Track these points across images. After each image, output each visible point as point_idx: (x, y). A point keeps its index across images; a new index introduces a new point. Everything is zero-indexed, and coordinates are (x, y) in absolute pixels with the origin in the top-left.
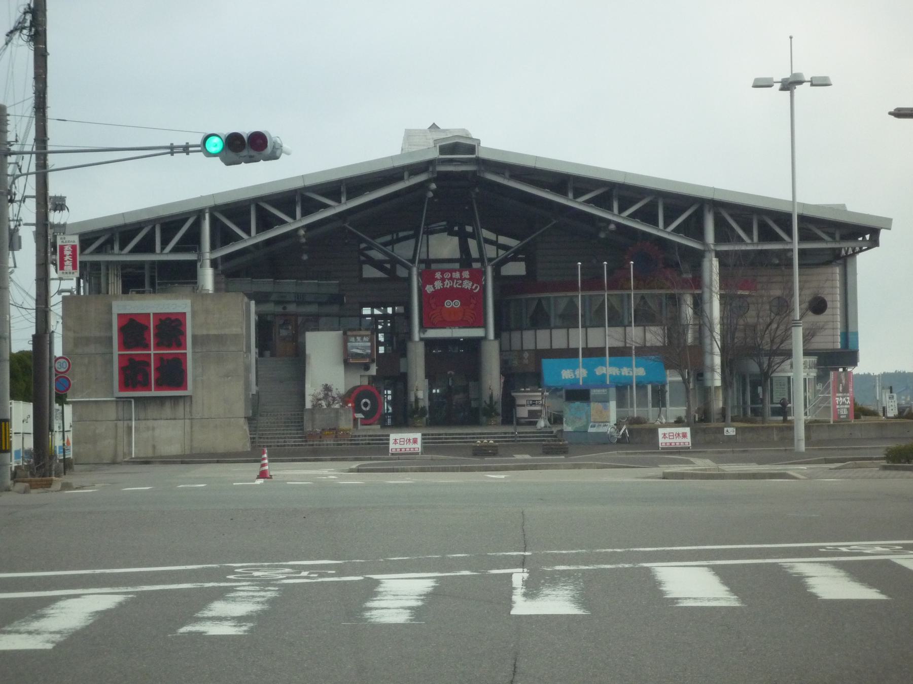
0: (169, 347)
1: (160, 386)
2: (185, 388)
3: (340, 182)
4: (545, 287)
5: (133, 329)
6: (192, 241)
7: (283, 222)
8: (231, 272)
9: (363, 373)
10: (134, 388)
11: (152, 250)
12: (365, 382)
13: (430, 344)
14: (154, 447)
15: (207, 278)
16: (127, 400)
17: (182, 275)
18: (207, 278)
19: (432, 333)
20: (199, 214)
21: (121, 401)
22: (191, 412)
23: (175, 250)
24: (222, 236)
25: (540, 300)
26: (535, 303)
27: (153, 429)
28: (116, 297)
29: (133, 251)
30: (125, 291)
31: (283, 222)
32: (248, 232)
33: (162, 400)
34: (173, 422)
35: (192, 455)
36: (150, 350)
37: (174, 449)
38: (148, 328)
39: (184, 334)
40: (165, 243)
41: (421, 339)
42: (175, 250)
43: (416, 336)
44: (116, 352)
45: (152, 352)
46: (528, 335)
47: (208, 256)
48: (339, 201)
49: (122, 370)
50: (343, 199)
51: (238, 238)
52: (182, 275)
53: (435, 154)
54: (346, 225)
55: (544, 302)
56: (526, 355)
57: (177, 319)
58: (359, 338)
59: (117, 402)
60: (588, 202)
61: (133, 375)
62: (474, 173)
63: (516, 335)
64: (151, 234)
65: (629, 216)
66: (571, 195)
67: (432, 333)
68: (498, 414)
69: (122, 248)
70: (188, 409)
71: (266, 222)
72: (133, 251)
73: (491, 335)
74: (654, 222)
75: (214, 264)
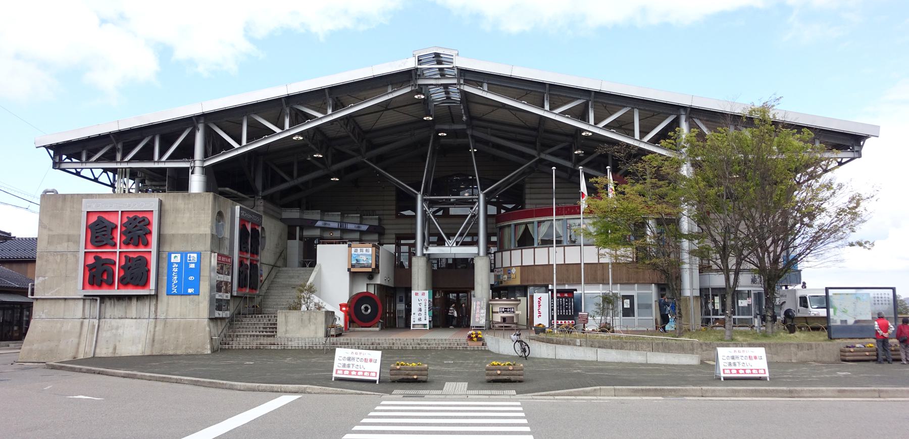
1: (124, 283)
4: (530, 214)
6: (186, 151)
8: (223, 180)
10: (100, 286)
11: (150, 159)
14: (115, 349)
15: (196, 182)
16: (93, 298)
18: (196, 182)
19: (434, 250)
20: (190, 122)
21: (86, 297)
22: (156, 312)
23: (172, 158)
24: (214, 145)
25: (526, 224)
26: (523, 227)
27: (117, 328)
31: (271, 133)
33: (130, 297)
34: (139, 320)
35: (152, 357)
37: (129, 349)
40: (162, 154)
43: (419, 253)
46: (516, 254)
47: (198, 164)
48: (324, 111)
50: (330, 112)
51: (229, 147)
52: (178, 182)
55: (530, 227)
56: (514, 271)
60: (563, 114)
61: (97, 273)
63: (506, 254)
66: (547, 107)
68: (186, 286)
69: (124, 155)
70: (153, 309)
71: (257, 132)
73: (482, 253)
74: (630, 133)
75: (206, 171)
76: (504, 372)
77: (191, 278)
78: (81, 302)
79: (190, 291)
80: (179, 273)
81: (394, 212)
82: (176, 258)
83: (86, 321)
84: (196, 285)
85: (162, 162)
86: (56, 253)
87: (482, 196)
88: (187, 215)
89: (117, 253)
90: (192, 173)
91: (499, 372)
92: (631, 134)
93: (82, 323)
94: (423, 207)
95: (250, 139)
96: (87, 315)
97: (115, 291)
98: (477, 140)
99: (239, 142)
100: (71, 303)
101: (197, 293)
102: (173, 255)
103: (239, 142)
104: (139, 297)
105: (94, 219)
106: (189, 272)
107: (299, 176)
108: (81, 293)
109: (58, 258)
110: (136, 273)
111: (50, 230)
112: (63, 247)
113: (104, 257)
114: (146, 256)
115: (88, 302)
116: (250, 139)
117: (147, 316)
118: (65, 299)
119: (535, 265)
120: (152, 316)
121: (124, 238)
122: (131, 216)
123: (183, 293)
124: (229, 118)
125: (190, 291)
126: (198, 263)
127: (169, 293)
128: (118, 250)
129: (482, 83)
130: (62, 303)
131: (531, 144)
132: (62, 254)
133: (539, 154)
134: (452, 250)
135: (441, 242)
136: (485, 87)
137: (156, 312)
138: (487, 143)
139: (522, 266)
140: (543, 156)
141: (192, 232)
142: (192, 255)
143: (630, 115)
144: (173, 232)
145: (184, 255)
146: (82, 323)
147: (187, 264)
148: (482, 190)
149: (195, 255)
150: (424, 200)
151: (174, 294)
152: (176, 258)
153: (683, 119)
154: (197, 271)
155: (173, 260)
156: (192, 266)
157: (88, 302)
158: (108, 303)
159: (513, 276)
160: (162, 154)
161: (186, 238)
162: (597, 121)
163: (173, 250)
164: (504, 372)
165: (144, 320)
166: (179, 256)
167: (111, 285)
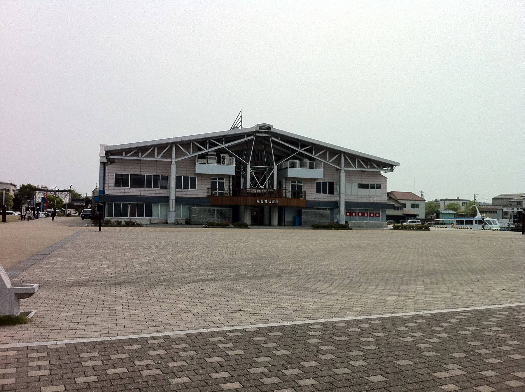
6: (169, 154)
47: (174, 160)
48: (222, 144)
64: (154, 150)
153: (342, 155)
160: (158, 156)
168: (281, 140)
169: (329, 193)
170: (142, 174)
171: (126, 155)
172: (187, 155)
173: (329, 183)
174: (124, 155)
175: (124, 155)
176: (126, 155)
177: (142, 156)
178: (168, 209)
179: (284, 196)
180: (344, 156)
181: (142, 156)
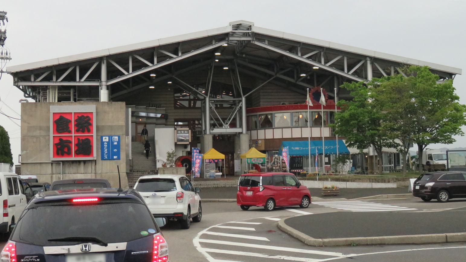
0: (83, 132)
1: (77, 154)
2: (92, 156)
3: (178, 44)
5: (61, 123)
6: (96, 76)
7: (147, 66)
9: (184, 150)
10: (62, 155)
11: (74, 80)
12: (185, 155)
13: (214, 137)
15: (104, 95)
16: (58, 163)
17: (91, 94)
18: (104, 95)
19: (218, 131)
20: (100, 59)
22: (95, 170)
23: (86, 80)
24: (112, 73)
28: (53, 104)
29: (63, 80)
30: (60, 100)
31: (147, 66)
32: (128, 70)
33: (79, 162)
34: (86, 174)
36: (72, 134)
38: (71, 122)
39: (91, 125)
40: (81, 78)
41: (210, 133)
42: (87, 80)
43: (208, 132)
44: (52, 135)
45: (73, 135)
47: (104, 83)
48: (177, 54)
49: (55, 145)
50: (180, 54)
52: (91, 94)
53: (229, 30)
54: (174, 76)
56: (260, 142)
57: (87, 117)
58: (182, 132)
59: (52, 164)
60: (308, 58)
61: (61, 148)
62: (250, 41)
64: (74, 71)
65: (330, 66)
66: (300, 54)
67: (218, 131)
69: (57, 78)
70: (93, 168)
72: (63, 80)
73: (244, 132)
75: (108, 87)
76: (331, 192)
77: (115, 150)
78: (50, 165)
79: (115, 157)
80: (108, 148)
81: (173, 105)
82: (106, 139)
83: (54, 176)
84: (118, 154)
85: (81, 82)
86: (33, 137)
87: (244, 99)
88: (111, 115)
89: (73, 135)
90: (101, 89)
91: (329, 192)
92: (343, 70)
93: (52, 177)
94: (209, 105)
95: (134, 70)
96: (54, 172)
97: (73, 158)
98: (239, 65)
99: (128, 71)
100: (44, 165)
101: (119, 158)
102: (104, 138)
103: (128, 71)
104: (85, 162)
105: (57, 117)
106: (114, 147)
107: (133, 86)
108: (52, 158)
109: (35, 140)
110: (85, 148)
111: (29, 123)
112: (37, 133)
113: (64, 139)
114: (90, 139)
115: (54, 165)
116: (134, 70)
117: (90, 172)
118: (41, 163)
119: (273, 139)
120: (94, 172)
121: (76, 128)
122: (80, 116)
123: (110, 158)
124: (122, 58)
125: (115, 157)
126: (119, 142)
127: (103, 159)
128: (73, 135)
129: (265, 40)
130: (39, 166)
131: (268, 66)
132: (37, 137)
133: (276, 74)
134: (226, 130)
135: (221, 126)
136: (267, 42)
137: (95, 170)
138: (244, 67)
139: (265, 140)
140: (278, 76)
141: (114, 124)
142: (115, 137)
143: (342, 60)
144: (103, 124)
145: (110, 137)
146: (52, 177)
147: (113, 143)
148: (244, 95)
149: (117, 137)
150: (210, 101)
151: (106, 159)
152: (106, 139)
153: (369, 62)
154: (118, 147)
155: (104, 140)
156: (116, 143)
157: (54, 165)
158: (67, 165)
159: (259, 145)
160: (81, 78)
161: (111, 128)
162: (326, 62)
163: (103, 134)
164: (331, 192)
165: (89, 174)
166: (107, 138)
167: (69, 154)
168: (270, 44)
169: (53, 136)
170: (94, 133)
171: (35, 80)
172: (123, 74)
173: (93, 136)
174: (32, 79)
175: (32, 79)
176: (35, 80)
177: (57, 79)
178: (69, 254)
179: (330, 128)
180: (372, 64)
181: (57, 79)
